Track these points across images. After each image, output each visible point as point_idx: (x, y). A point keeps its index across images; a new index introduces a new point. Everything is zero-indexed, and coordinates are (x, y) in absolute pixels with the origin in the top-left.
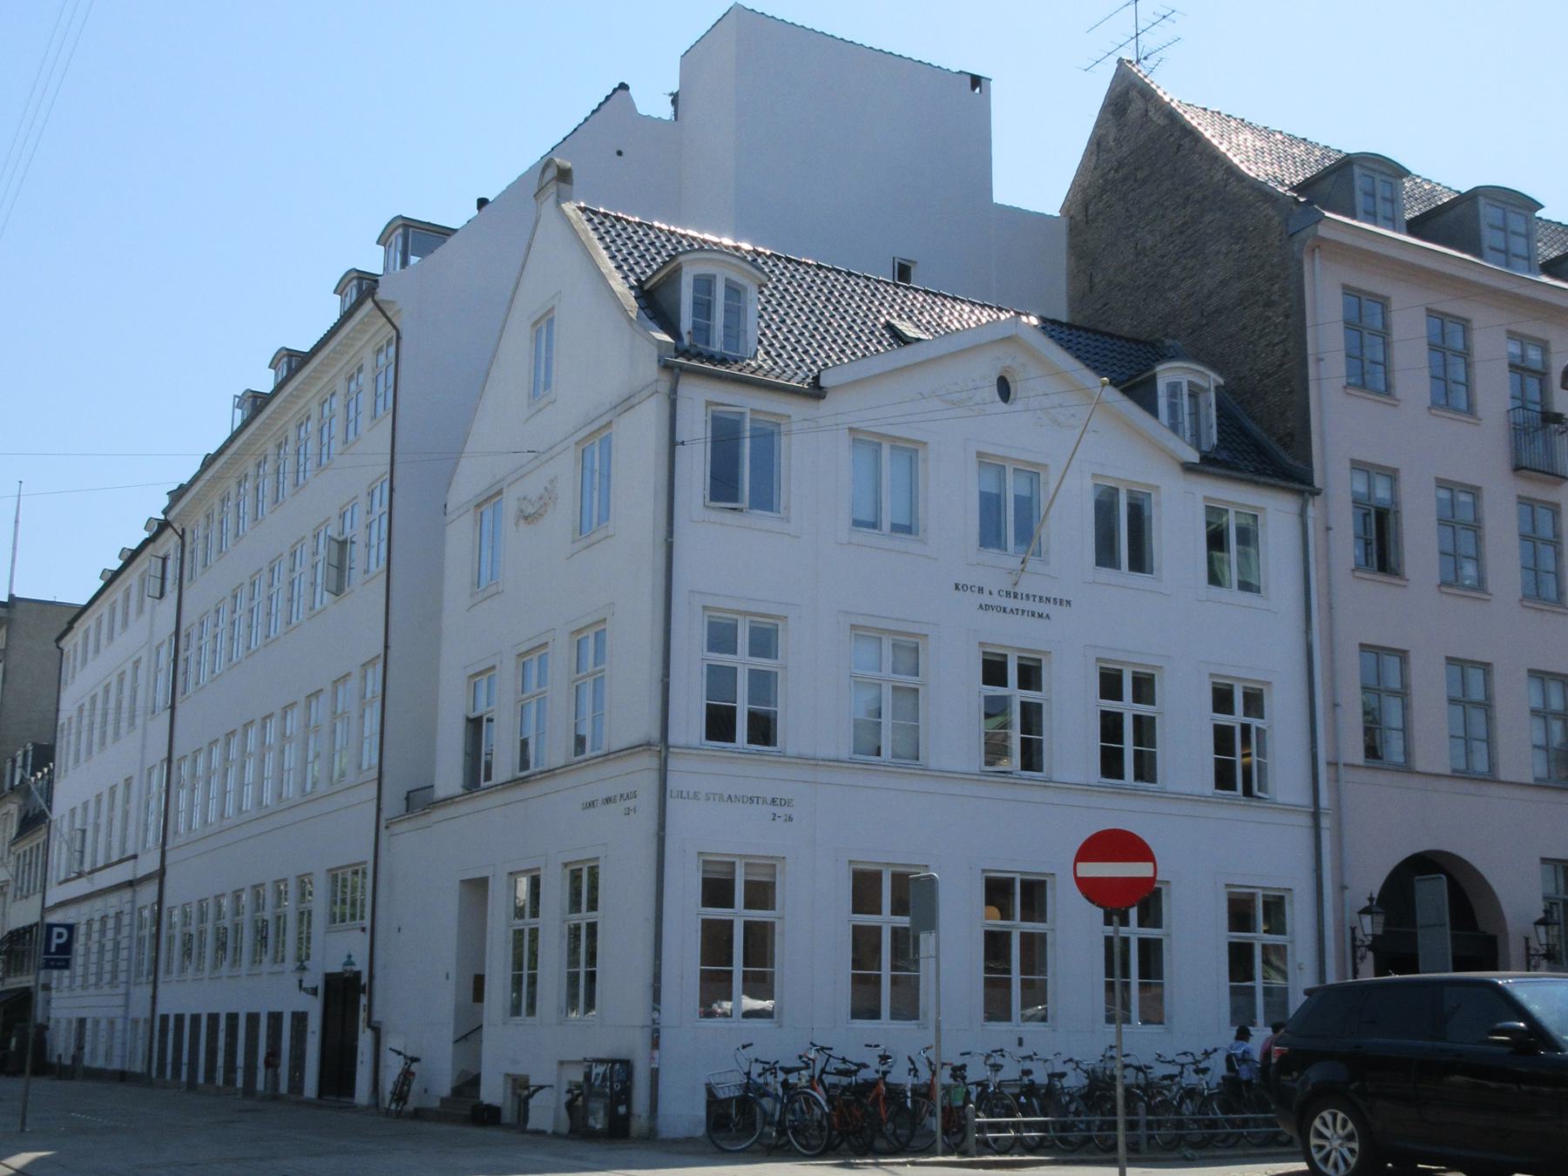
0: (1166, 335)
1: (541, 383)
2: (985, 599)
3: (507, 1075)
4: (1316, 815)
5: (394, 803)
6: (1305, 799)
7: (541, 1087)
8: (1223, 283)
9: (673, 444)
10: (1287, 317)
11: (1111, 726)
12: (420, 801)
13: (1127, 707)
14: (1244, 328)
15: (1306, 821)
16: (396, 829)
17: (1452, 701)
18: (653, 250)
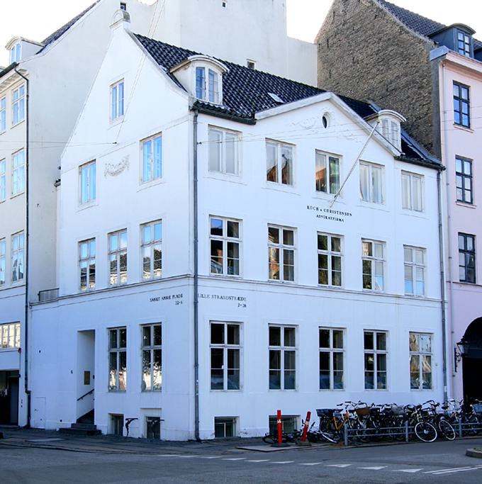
0: (369, 99)
1: (119, 110)
2: (319, 213)
3: (110, 414)
4: (443, 302)
5: (33, 297)
6: (439, 298)
7: (133, 419)
8: (398, 77)
9: (196, 144)
10: (430, 93)
11: (322, 260)
12: (48, 296)
13: (329, 252)
14: (408, 97)
15: (439, 305)
16: (34, 308)
17: (460, 251)
18: (175, 57)
